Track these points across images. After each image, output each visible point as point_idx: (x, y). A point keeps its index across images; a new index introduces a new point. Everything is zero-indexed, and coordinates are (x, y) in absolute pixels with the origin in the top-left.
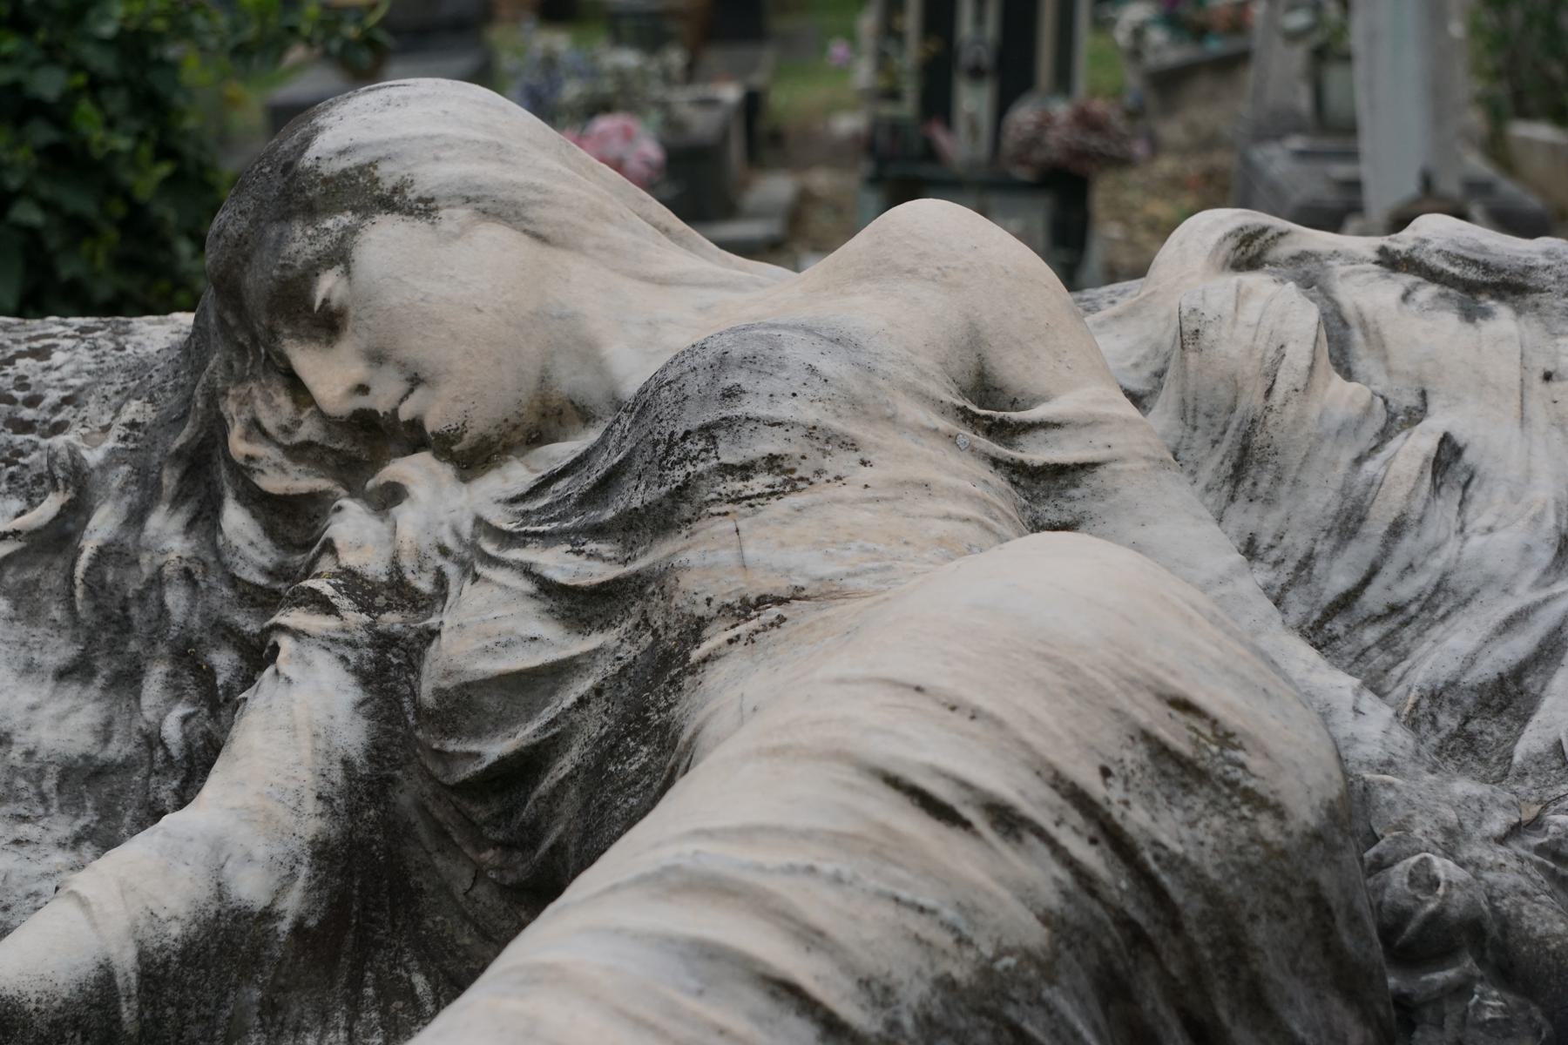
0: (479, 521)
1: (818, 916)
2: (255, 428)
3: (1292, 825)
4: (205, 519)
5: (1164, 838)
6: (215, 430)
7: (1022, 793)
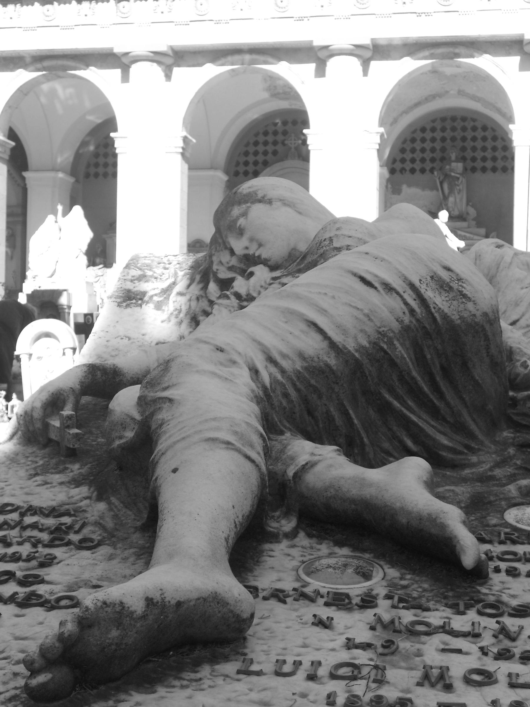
1: (325, 306)
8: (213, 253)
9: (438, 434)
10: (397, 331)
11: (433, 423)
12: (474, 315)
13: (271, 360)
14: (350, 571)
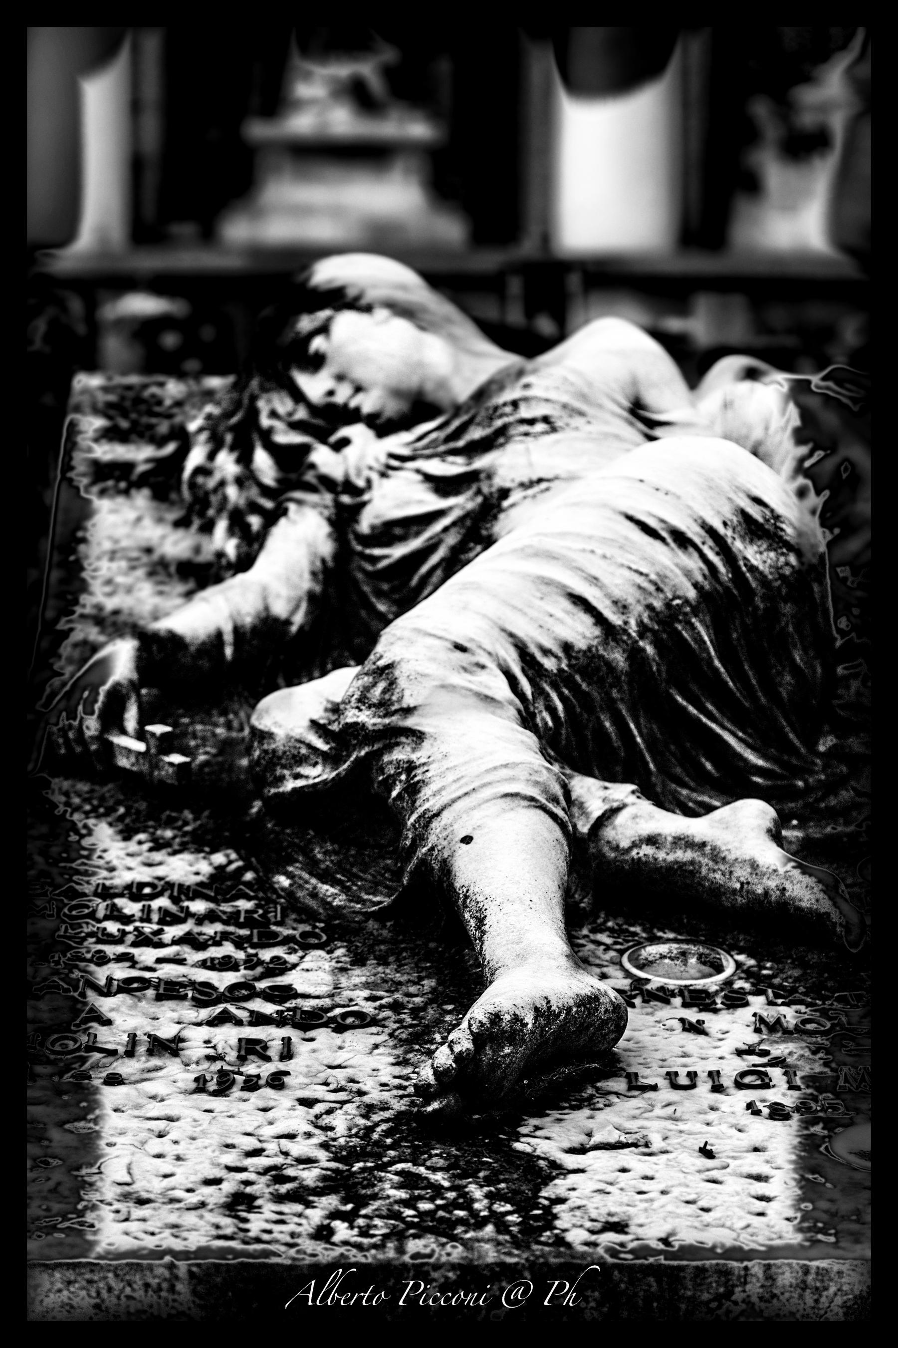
2: (273, 414)
3: (804, 560)
4: (245, 459)
5: (749, 557)
6: (254, 413)
7: (688, 528)
14: (693, 961)
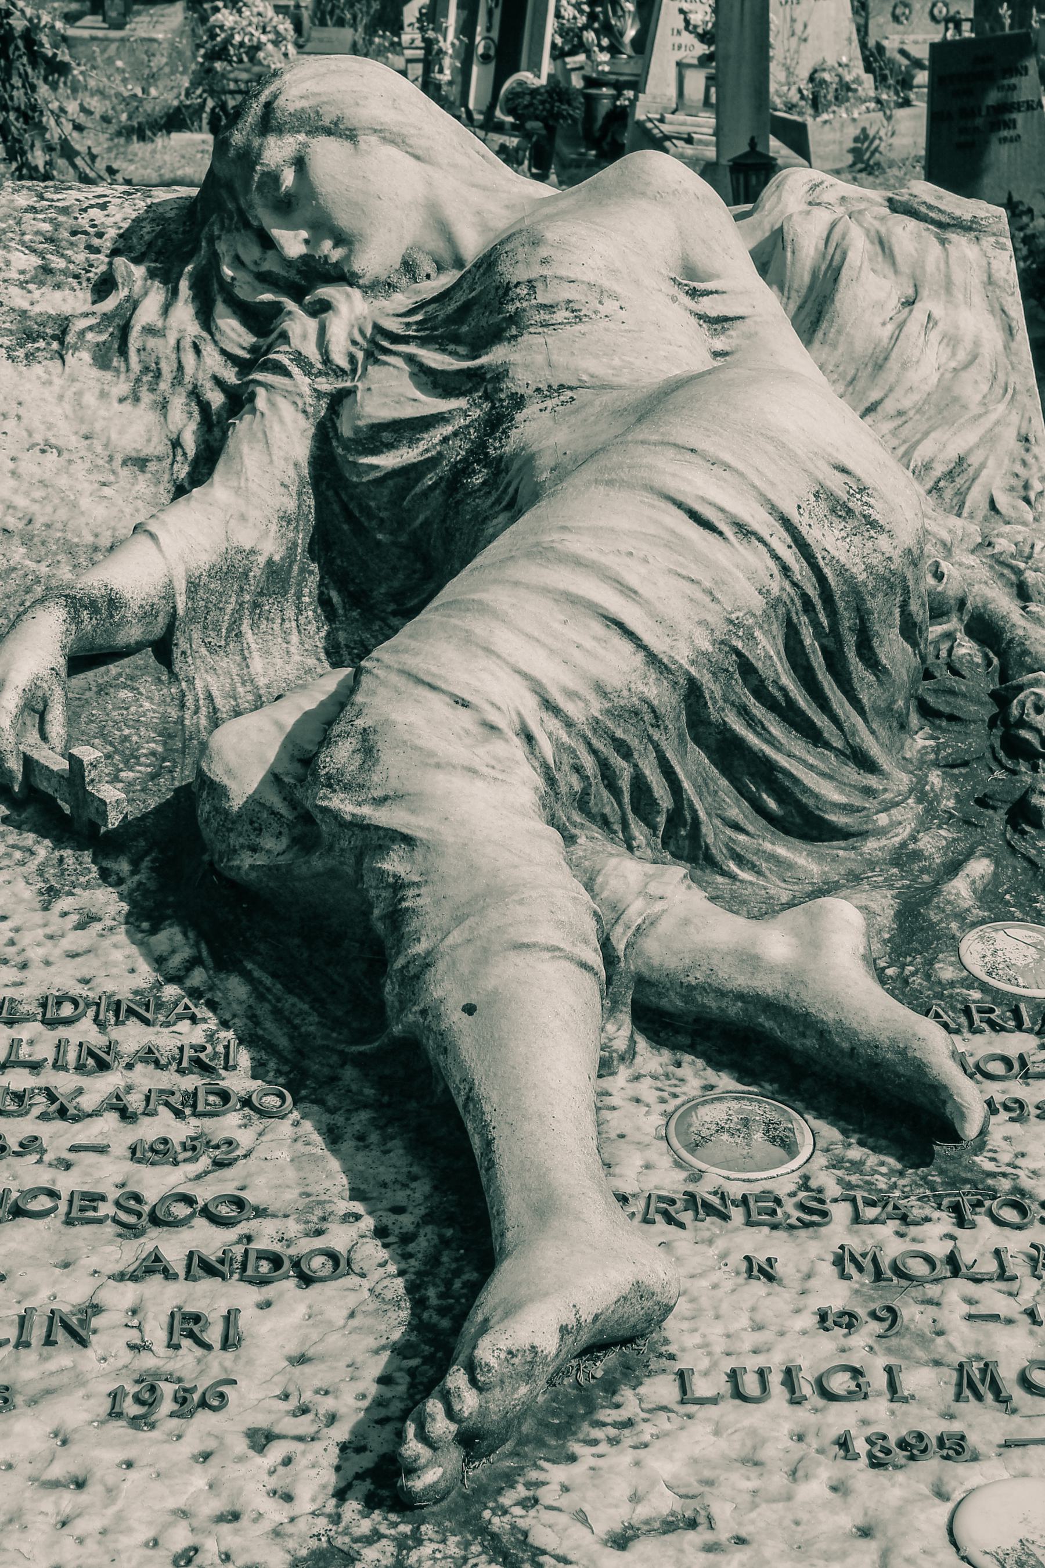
0: (378, 328)
2: (238, 262)
8: (216, 233)
9: (821, 781)
10: (759, 613)
11: (811, 760)
12: (890, 558)
13: (549, 706)
